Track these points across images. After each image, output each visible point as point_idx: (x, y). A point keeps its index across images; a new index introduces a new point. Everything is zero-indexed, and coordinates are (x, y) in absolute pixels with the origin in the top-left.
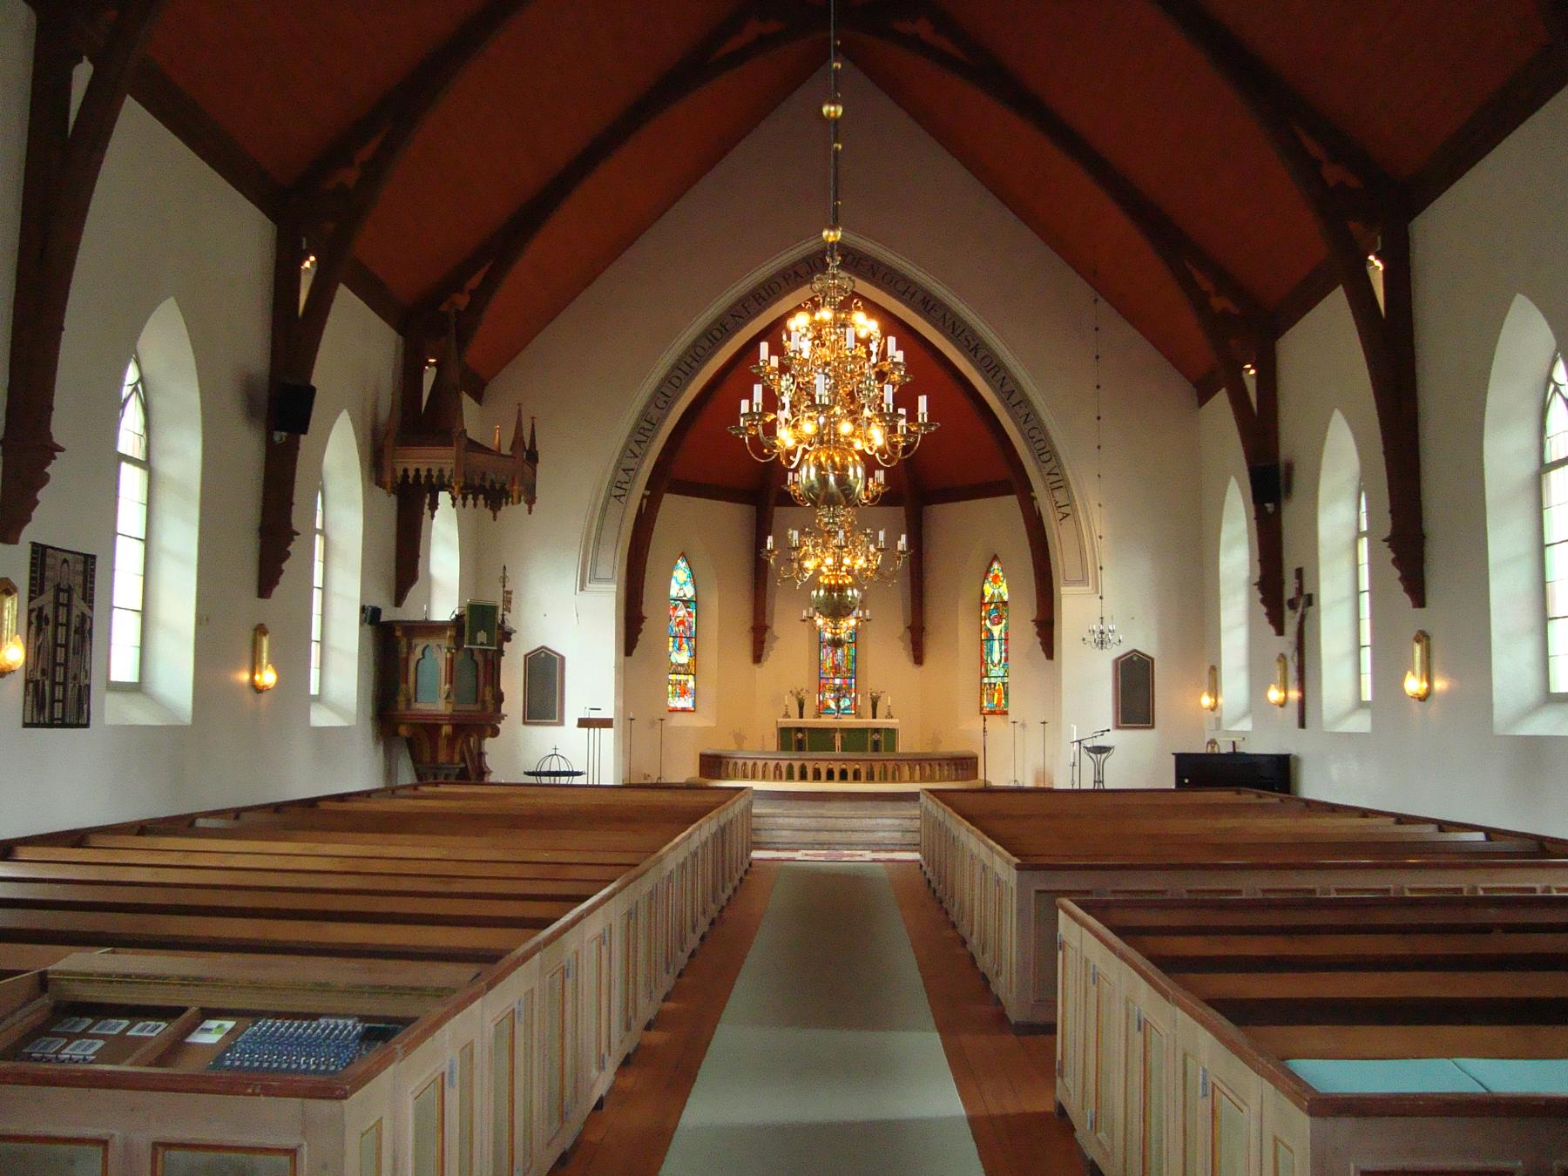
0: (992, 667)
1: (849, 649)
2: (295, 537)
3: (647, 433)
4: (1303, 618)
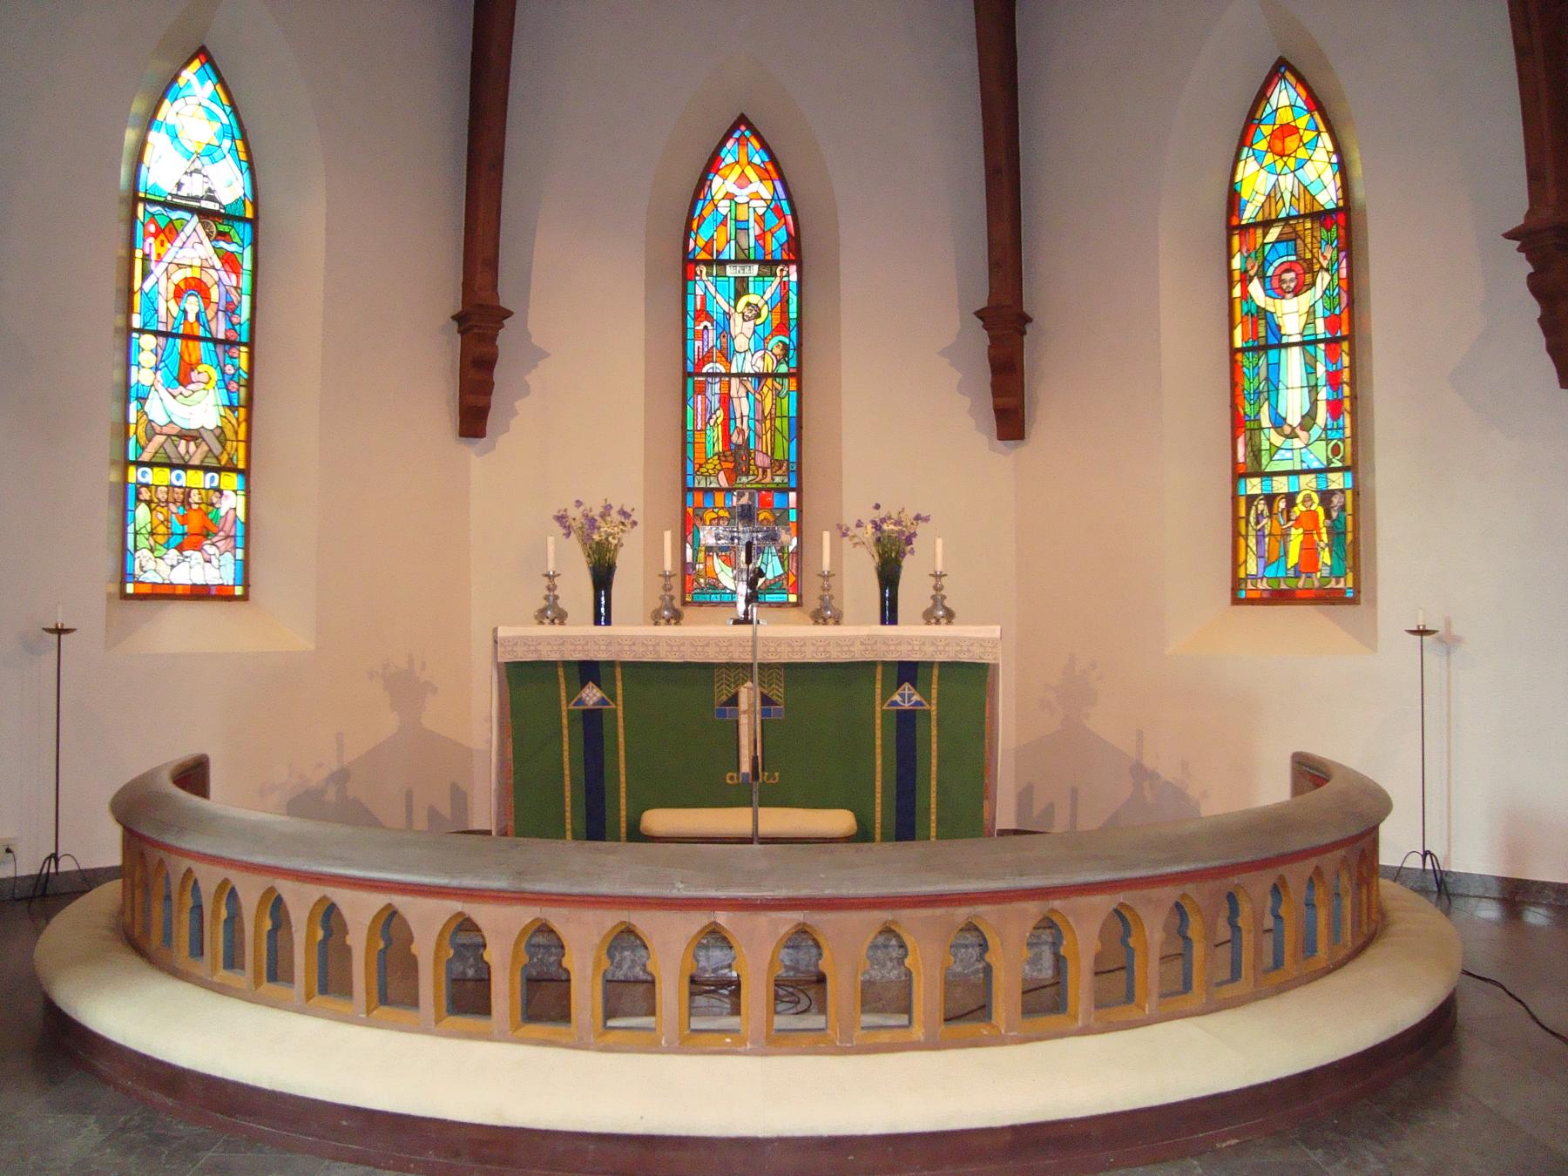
0: (1277, 440)
1: (777, 394)
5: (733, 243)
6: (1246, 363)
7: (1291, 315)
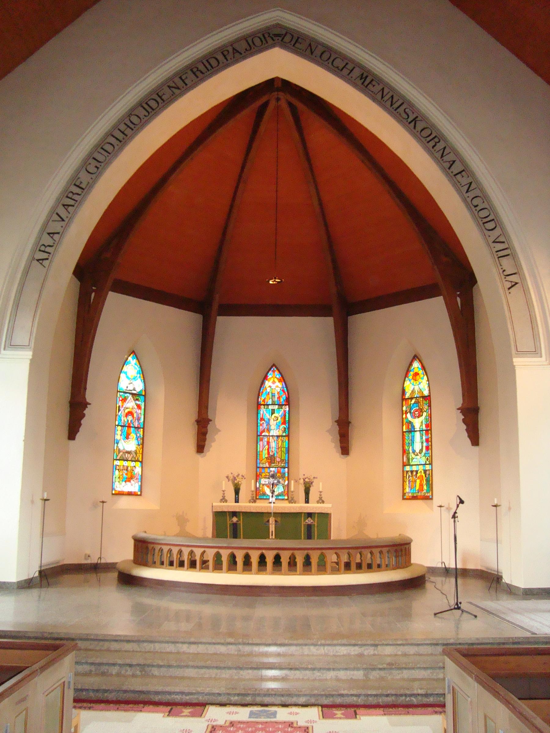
0: (413, 456)
1: (282, 441)
3: (76, 197)
5: (271, 399)
6: (406, 435)
7: (418, 423)
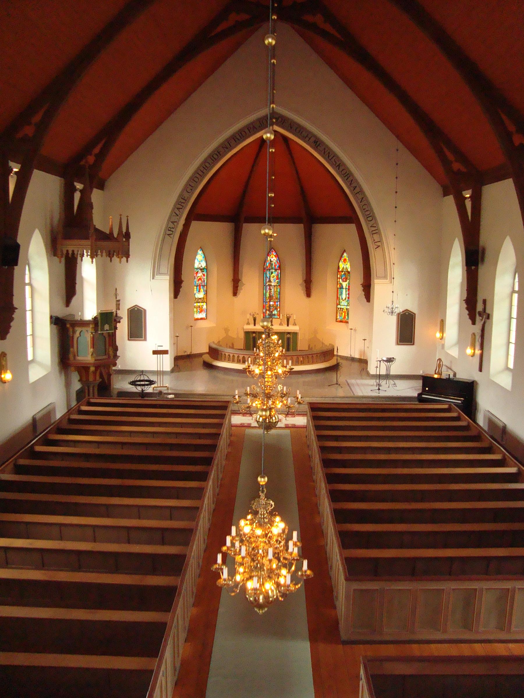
0: (342, 301)
1: (277, 288)
2: (16, 310)
3: (182, 204)
4: (484, 323)
7: (345, 284)
